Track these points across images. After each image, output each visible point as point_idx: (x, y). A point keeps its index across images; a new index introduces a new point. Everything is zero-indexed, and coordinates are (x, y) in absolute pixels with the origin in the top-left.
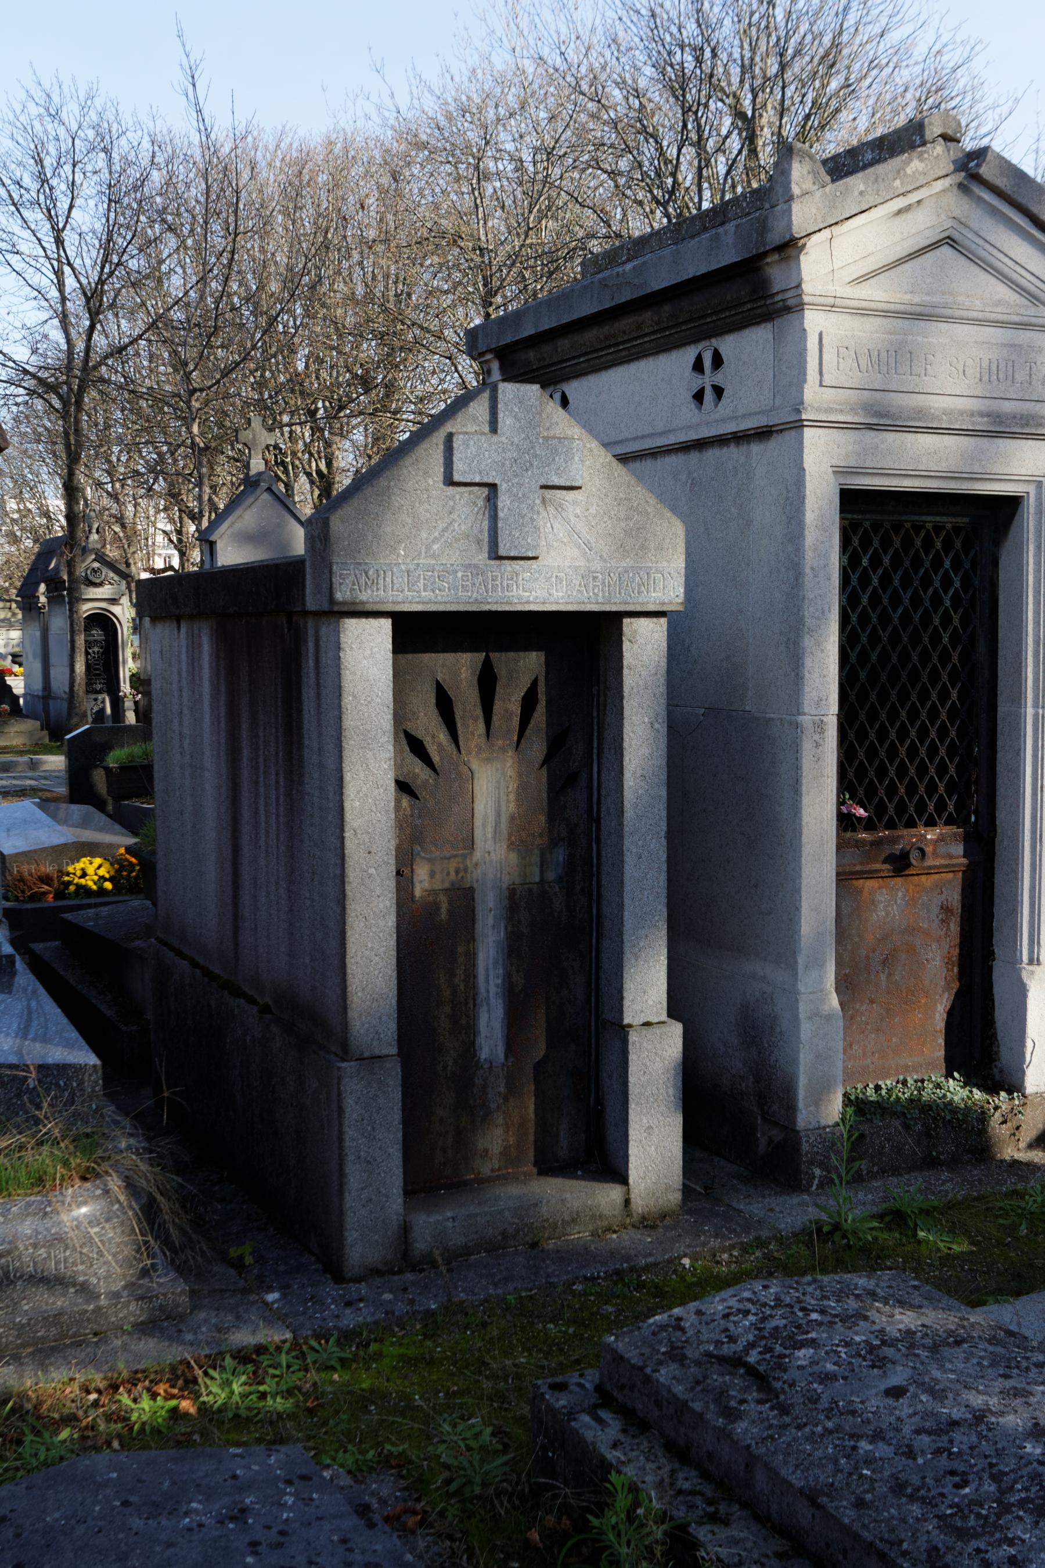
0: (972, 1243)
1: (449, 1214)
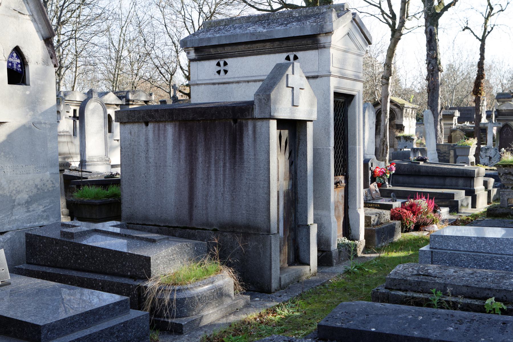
0: (377, 270)
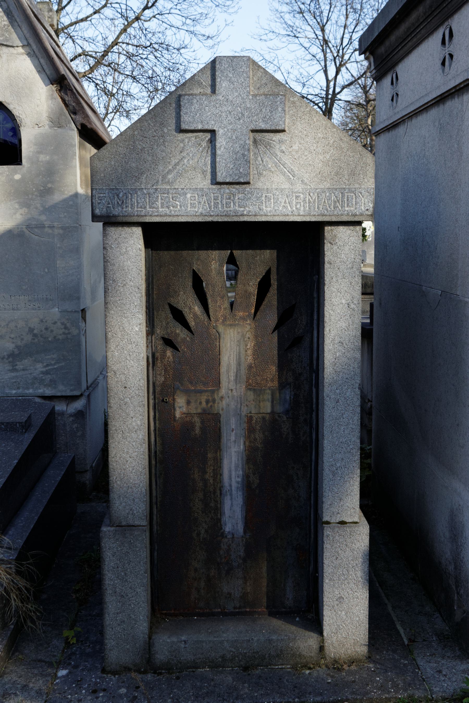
1: (183, 638)
